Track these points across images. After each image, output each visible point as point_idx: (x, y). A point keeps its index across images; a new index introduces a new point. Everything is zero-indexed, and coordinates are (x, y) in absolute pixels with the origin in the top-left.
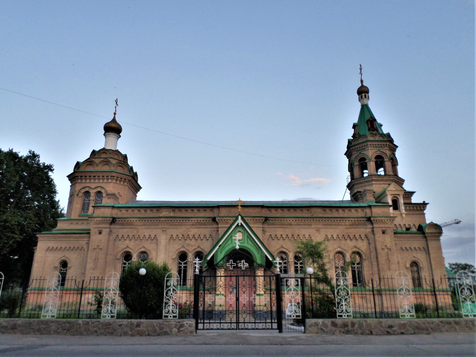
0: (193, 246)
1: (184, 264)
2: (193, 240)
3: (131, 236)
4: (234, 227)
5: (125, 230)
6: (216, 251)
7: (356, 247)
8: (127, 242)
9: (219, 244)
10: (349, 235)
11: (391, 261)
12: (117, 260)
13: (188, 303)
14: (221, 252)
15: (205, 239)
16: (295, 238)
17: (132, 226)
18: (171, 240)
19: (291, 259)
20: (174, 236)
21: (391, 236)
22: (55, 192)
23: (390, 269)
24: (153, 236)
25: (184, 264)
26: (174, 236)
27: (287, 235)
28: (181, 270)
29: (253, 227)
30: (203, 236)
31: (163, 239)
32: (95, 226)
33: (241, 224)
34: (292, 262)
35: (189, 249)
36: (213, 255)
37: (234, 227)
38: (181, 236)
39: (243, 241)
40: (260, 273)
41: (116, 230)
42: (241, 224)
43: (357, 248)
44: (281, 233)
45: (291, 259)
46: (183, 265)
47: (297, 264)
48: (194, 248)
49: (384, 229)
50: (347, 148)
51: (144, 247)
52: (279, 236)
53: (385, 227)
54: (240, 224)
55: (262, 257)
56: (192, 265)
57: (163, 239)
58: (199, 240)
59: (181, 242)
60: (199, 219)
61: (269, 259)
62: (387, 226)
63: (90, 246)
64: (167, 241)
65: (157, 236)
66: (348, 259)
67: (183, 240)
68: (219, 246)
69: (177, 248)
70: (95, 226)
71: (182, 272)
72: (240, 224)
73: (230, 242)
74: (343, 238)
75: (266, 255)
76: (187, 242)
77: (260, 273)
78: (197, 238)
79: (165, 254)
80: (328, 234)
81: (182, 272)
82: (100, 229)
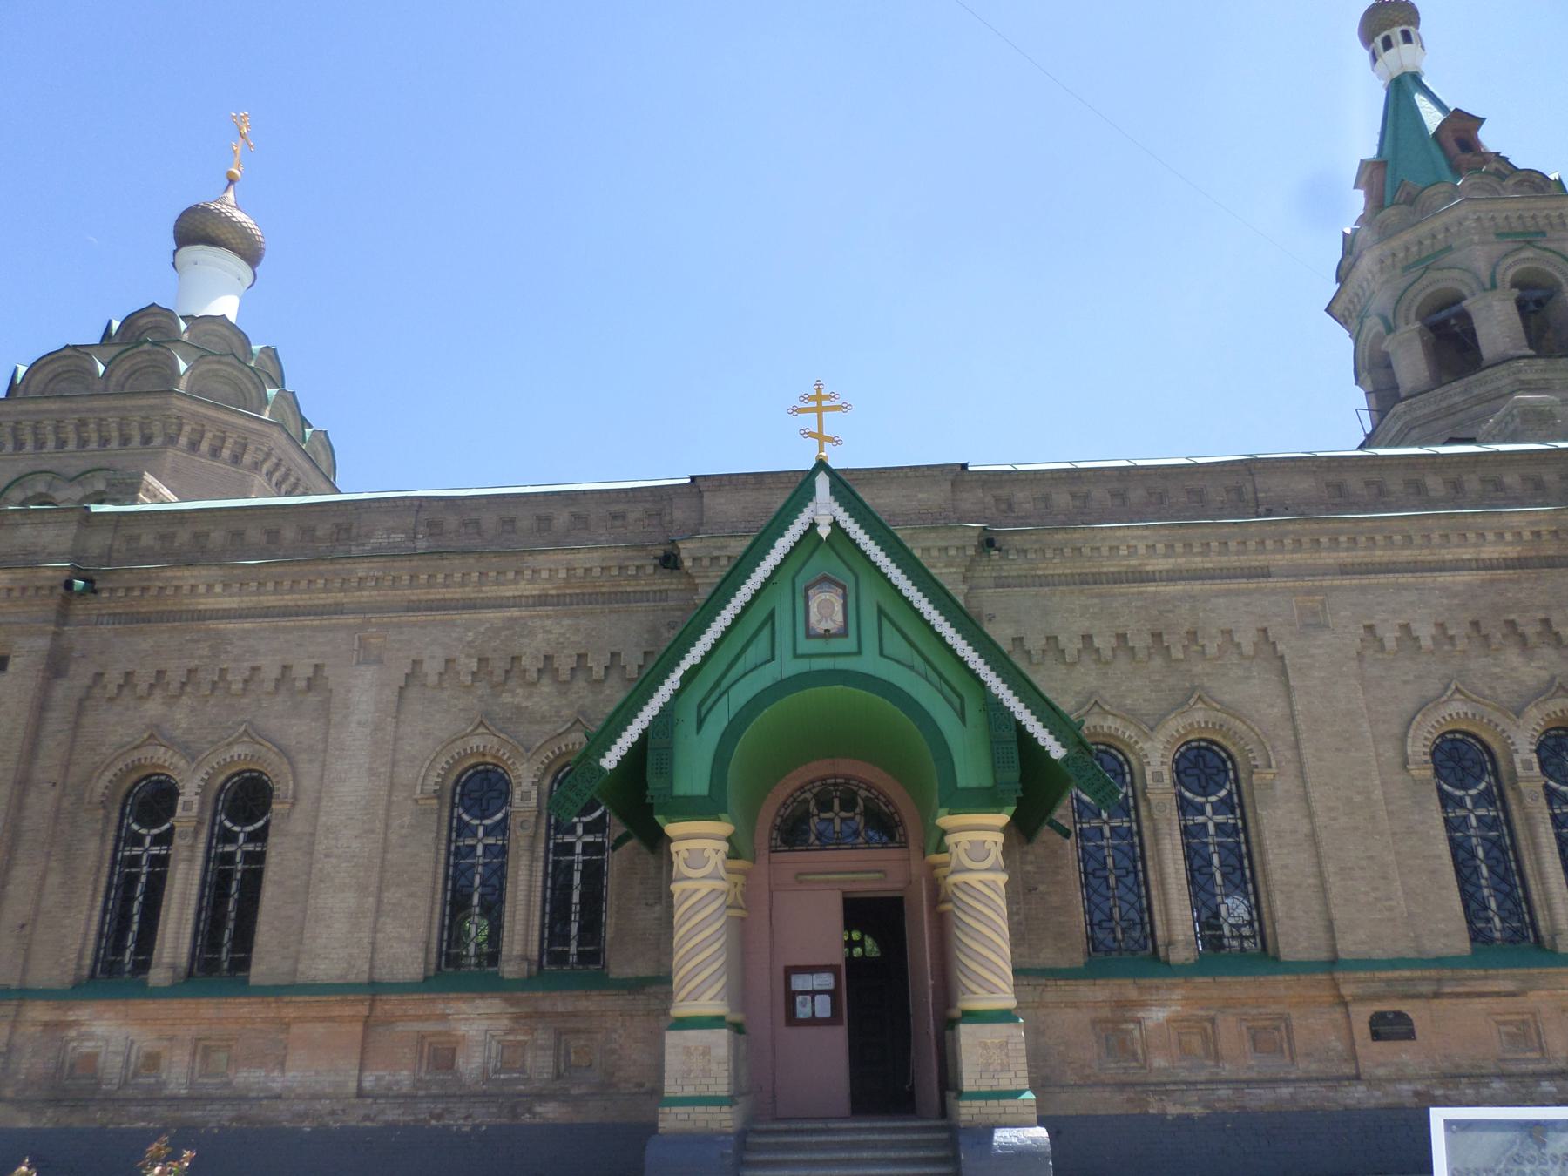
1: (251, 837)
2: (546, 687)
3: (176, 676)
4: (783, 545)
6: (667, 711)
8: (153, 708)
9: (685, 665)
14: (700, 722)
16: (1177, 653)
19: (1158, 777)
20: (432, 668)
24: (303, 671)
26: (432, 668)
27: (1122, 637)
28: (137, 877)
31: (363, 694)
33: (835, 524)
36: (644, 736)
37: (783, 545)
38: (474, 665)
39: (849, 644)
42: (835, 524)
44: (1082, 625)
47: (137, 840)
50: (1338, 279)
51: (253, 734)
52: (1072, 646)
54: (824, 531)
55: (994, 743)
57: (363, 694)
58: (580, 683)
61: (1043, 753)
64: (391, 694)
65: (327, 672)
68: (688, 678)
72: (824, 531)
73: (759, 649)
75: (1020, 727)
76: (506, 698)
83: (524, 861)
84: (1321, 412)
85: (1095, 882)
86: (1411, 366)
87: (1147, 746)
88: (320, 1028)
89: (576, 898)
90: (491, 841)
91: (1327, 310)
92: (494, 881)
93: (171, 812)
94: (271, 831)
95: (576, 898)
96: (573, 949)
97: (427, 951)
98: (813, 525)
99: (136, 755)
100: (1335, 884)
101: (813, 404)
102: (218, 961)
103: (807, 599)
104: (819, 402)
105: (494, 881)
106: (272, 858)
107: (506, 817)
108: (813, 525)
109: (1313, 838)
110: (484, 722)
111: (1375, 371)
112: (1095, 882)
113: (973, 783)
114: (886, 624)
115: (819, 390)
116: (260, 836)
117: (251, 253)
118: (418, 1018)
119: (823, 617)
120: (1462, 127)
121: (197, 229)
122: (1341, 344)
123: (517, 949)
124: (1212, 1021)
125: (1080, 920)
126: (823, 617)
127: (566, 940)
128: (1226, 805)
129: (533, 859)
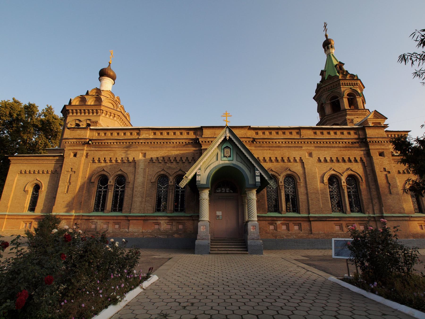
0: (174, 169)
1: (121, 188)
2: (174, 163)
5: (102, 153)
7: (163, 170)
10: (343, 158)
11: (391, 184)
12: (91, 184)
13: (32, 230)
15: (187, 162)
17: (109, 149)
18: (151, 163)
21: (389, 158)
22: (30, 109)
23: (391, 193)
25: (122, 188)
28: (118, 194)
29: (251, 150)
30: (185, 159)
32: (69, 148)
33: (229, 137)
34: (282, 185)
35: (169, 172)
40: (253, 196)
41: (92, 152)
43: (334, 170)
44: (269, 156)
45: (281, 182)
46: (163, 190)
47: (118, 188)
48: (175, 171)
49: (381, 151)
53: (145, 150)
56: (172, 189)
59: (161, 165)
60: (181, 141)
62: (383, 147)
63: (63, 168)
66: (344, 182)
67: (163, 163)
69: (157, 171)
70: (69, 148)
71: (180, 197)
74: (157, 161)
76: (168, 165)
77: (253, 196)
78: (178, 161)
79: (144, 177)
80: (106, 157)
81: (180, 197)
82: (75, 151)
83: (171, 193)
84: (311, 117)
85: (269, 200)
86: (328, 110)
87: (280, 177)
88: (135, 221)
89: (180, 200)
90: (164, 190)
91: (314, 98)
92: (165, 197)
93: (107, 183)
94: (126, 187)
95: (180, 200)
96: (179, 209)
97: (154, 208)
98: (226, 137)
99: (100, 173)
100: (310, 202)
101: (225, 115)
102: (117, 209)
103: (224, 150)
104: (226, 115)
105: (165, 197)
106: (126, 191)
107: (124, 186)
108: (226, 137)
109: (307, 194)
110: (163, 170)
111: (321, 110)
112: (269, 200)
113: (252, 183)
114: (238, 155)
115: (226, 112)
116: (124, 187)
117: (113, 78)
118: (152, 220)
119: (227, 154)
120: (341, 64)
121: (103, 73)
122: (315, 105)
123: (170, 208)
124: (288, 224)
125: (267, 207)
126: (227, 154)
127: (178, 207)
128: (105, 188)
129: (172, 193)
